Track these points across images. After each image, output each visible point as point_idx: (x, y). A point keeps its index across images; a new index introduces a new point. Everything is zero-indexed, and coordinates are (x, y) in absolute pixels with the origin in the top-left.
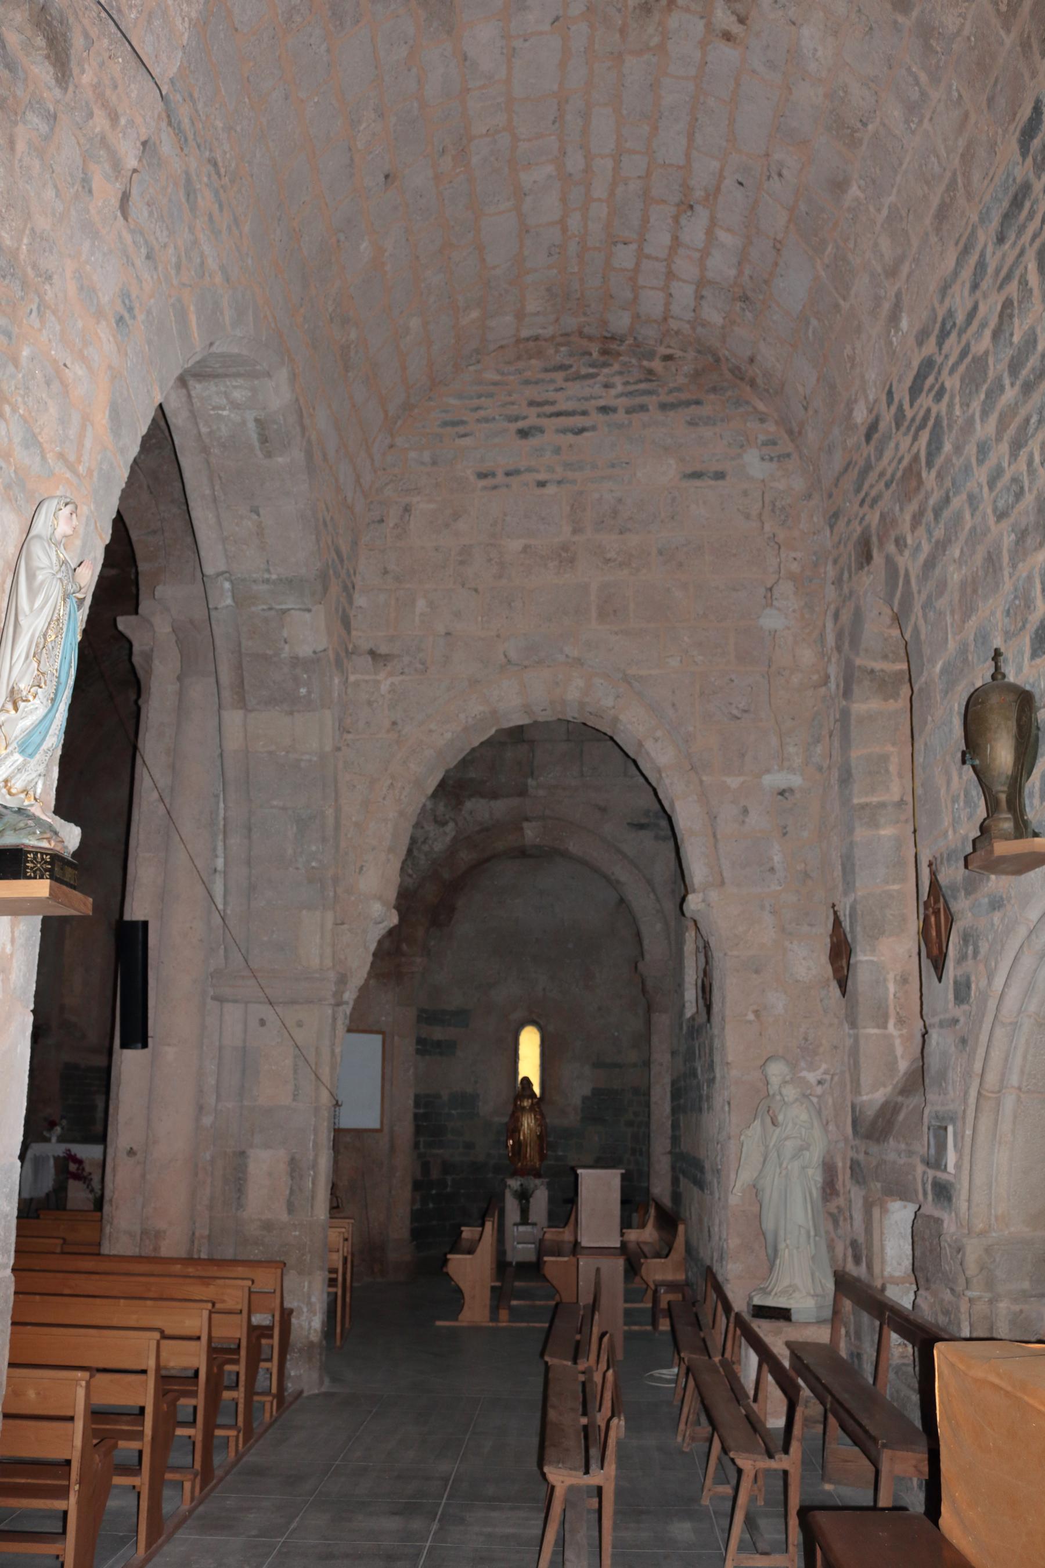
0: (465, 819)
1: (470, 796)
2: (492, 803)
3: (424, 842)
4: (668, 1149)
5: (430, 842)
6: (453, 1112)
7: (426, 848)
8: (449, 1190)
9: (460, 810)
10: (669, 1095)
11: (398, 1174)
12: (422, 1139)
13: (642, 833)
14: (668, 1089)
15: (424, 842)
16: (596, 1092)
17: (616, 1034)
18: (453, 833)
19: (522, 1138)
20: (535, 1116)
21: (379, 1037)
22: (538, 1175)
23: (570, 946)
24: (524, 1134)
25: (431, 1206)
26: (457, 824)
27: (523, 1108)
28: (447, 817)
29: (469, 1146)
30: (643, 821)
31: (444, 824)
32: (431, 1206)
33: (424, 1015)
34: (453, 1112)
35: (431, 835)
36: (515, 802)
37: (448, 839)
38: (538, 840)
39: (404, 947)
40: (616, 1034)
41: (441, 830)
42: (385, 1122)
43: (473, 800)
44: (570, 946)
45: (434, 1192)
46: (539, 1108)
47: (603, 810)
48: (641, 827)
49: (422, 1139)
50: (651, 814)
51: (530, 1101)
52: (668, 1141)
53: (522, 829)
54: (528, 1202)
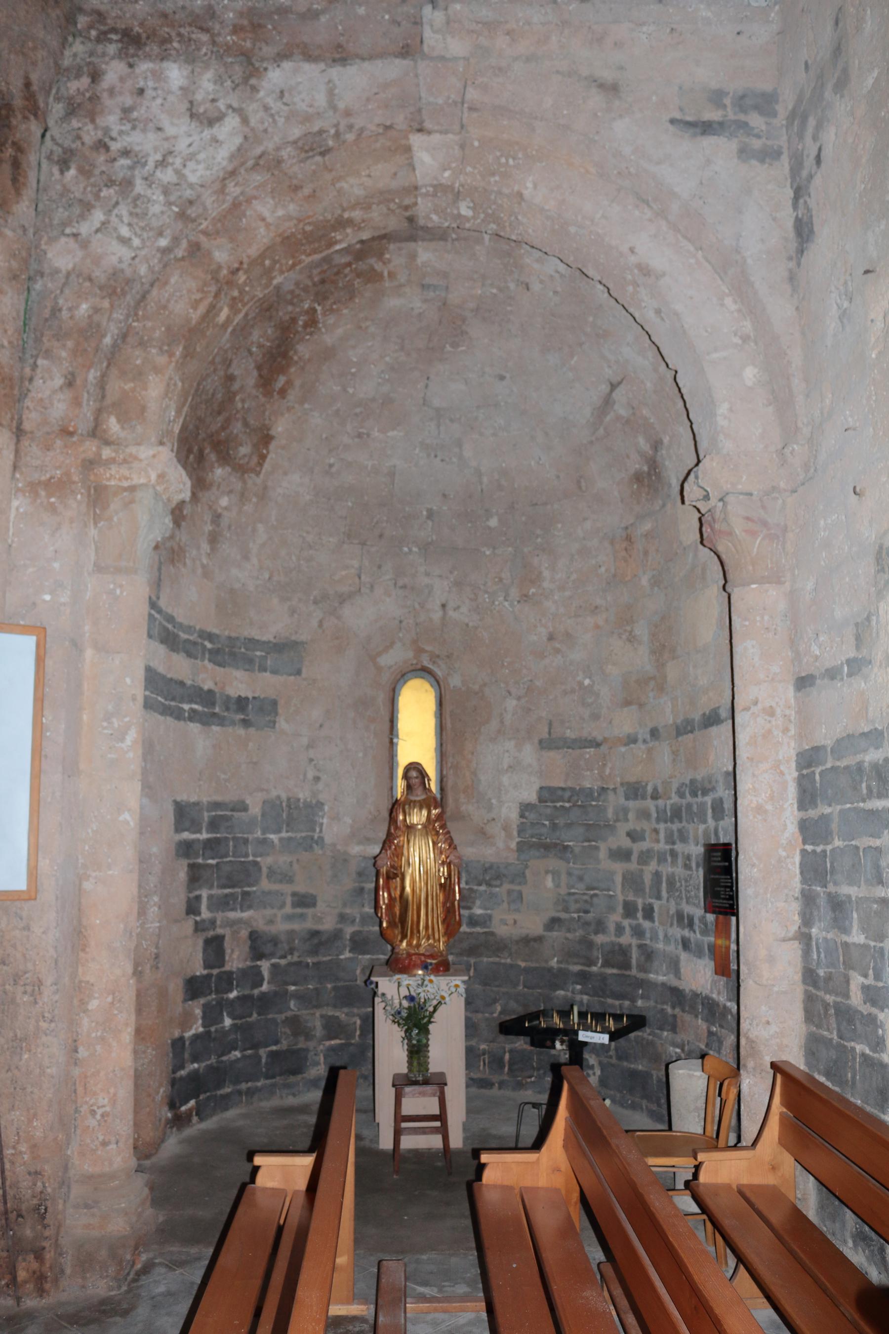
0: (266, 108)
1: (282, 56)
2: (335, 72)
3: (162, 163)
4: (794, 928)
5: (178, 161)
6: (272, 836)
7: (167, 176)
8: (265, 987)
9: (254, 89)
10: (792, 791)
11: (93, 1004)
12: (204, 893)
13: (709, 141)
14: (791, 774)
15: (162, 163)
16: (548, 794)
17: (587, 682)
18: (238, 140)
19: (408, 889)
20: (434, 844)
21: (29, 643)
22: (443, 967)
23: (493, 522)
24: (413, 882)
25: (228, 1022)
26: (245, 121)
27: (410, 828)
28: (221, 105)
29: (304, 901)
30: (712, 115)
31: (212, 121)
32: (228, 1022)
33: (209, 645)
34: (272, 836)
35: (182, 145)
36: (393, 69)
37: (222, 155)
38: (447, 174)
39: (113, 424)
40: (587, 682)
41: (207, 134)
42: (44, 864)
43: (287, 65)
44: (493, 522)
45: (233, 995)
46: (443, 827)
47: (611, 89)
48: (706, 128)
49: (204, 893)
50: (727, 101)
51: (425, 813)
52: (795, 908)
53: (408, 149)
54: (424, 1030)
